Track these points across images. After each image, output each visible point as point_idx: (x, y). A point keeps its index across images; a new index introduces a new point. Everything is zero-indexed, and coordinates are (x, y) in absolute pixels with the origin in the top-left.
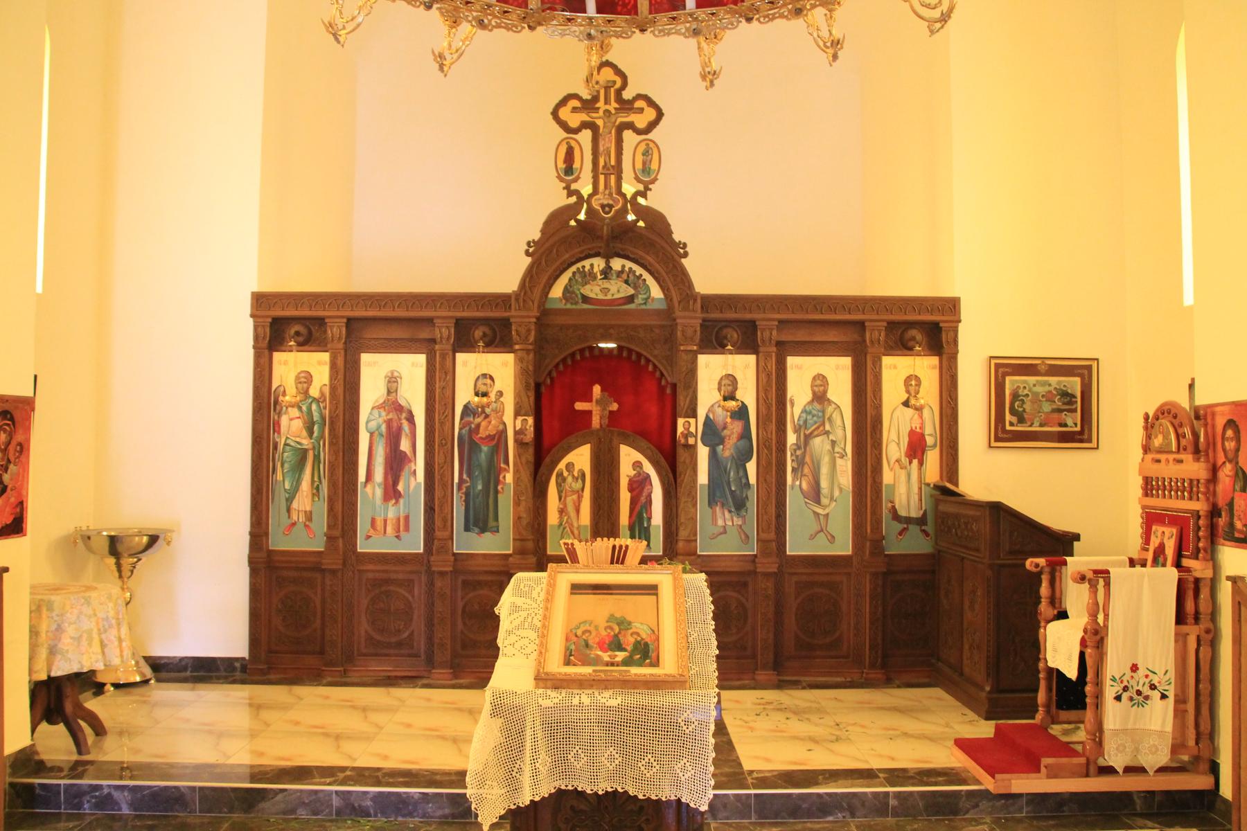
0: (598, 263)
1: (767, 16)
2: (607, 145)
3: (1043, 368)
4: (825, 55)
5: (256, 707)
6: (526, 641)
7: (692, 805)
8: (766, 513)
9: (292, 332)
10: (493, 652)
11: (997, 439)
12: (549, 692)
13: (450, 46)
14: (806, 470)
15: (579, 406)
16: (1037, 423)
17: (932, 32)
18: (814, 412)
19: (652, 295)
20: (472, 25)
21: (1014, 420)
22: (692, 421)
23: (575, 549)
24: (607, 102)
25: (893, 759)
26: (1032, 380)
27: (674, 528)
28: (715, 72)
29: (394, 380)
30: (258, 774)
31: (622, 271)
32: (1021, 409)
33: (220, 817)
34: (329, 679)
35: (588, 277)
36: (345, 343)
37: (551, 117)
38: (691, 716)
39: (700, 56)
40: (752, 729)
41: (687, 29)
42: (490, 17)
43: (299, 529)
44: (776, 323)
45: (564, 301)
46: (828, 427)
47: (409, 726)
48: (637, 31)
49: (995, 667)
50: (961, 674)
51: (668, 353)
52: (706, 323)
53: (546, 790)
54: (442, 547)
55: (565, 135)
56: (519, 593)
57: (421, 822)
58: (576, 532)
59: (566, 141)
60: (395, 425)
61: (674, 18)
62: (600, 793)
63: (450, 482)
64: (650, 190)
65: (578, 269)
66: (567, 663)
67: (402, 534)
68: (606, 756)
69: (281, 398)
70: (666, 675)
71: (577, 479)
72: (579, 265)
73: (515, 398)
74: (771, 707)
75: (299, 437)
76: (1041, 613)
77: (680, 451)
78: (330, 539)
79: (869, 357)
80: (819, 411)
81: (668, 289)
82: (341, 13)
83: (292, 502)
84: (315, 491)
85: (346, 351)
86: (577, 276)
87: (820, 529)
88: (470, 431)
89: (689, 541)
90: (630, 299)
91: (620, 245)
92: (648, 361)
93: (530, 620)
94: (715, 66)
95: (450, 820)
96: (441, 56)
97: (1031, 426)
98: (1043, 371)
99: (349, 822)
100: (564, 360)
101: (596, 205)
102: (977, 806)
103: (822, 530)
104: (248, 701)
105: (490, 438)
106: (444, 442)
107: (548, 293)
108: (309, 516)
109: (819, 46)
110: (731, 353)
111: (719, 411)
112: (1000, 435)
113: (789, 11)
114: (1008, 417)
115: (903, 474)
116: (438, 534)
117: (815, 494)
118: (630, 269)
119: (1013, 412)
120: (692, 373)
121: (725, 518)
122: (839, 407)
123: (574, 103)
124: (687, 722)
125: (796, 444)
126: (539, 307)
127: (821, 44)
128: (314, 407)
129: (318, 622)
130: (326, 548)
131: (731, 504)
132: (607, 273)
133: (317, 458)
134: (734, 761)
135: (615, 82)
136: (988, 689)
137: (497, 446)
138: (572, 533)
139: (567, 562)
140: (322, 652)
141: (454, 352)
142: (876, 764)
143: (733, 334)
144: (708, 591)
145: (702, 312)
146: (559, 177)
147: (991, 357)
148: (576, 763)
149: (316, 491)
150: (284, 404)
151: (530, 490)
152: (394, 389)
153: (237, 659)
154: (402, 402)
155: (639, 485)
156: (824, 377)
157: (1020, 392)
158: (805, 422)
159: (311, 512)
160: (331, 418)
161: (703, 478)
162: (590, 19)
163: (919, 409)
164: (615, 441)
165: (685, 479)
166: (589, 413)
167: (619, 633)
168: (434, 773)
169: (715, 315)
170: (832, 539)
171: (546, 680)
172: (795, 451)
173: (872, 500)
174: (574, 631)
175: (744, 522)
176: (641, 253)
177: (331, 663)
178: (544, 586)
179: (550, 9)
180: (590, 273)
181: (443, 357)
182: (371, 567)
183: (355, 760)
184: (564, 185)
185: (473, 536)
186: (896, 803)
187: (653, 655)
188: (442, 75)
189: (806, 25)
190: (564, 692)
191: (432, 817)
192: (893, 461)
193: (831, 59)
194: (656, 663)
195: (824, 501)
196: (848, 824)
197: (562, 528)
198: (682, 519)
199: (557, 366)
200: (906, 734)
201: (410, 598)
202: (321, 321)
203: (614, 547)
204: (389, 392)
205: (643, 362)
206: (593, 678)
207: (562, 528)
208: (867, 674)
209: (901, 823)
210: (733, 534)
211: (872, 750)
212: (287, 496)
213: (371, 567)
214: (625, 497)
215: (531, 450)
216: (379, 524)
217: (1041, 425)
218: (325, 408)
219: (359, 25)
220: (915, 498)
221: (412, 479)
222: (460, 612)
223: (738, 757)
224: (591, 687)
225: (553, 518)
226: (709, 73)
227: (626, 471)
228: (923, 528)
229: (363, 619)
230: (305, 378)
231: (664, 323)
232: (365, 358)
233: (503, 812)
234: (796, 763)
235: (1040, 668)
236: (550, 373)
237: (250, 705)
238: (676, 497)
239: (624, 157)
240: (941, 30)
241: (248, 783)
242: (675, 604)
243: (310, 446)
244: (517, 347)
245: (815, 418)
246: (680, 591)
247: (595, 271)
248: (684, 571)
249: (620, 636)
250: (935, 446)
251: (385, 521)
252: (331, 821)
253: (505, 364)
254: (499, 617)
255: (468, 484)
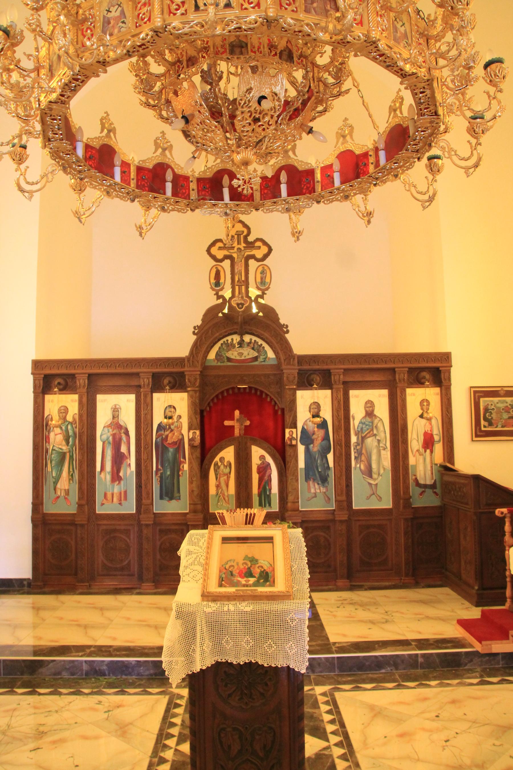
0: (236, 338)
1: (329, 200)
2: (239, 269)
3: (502, 393)
4: (363, 221)
5: (37, 609)
6: (196, 572)
7: (296, 669)
8: (340, 484)
9: (56, 383)
10: (177, 579)
11: (477, 436)
12: (210, 603)
13: (145, 221)
14: (363, 458)
15: (227, 423)
16: (500, 426)
17: (424, 208)
18: (367, 423)
19: (268, 356)
20: (158, 210)
21: (486, 424)
22: (294, 430)
23: (224, 516)
24: (239, 243)
25: (420, 633)
26: (496, 400)
27: (285, 495)
28: (300, 231)
29: (116, 410)
30: (38, 651)
31: (250, 343)
32: (490, 418)
33: (15, 678)
34: (80, 591)
35: (230, 346)
36: (87, 388)
37: (206, 253)
38: (294, 616)
39: (291, 223)
40: (335, 616)
41: (283, 208)
42: (168, 205)
43: (62, 500)
44: (342, 371)
45: (216, 361)
46: (375, 432)
47: (128, 619)
48: (254, 210)
49: (480, 575)
50: (460, 579)
51: (279, 390)
52: (301, 372)
53: (209, 662)
54: (147, 509)
55: (215, 263)
56: (191, 543)
57: (136, 679)
58: (226, 498)
59: (215, 267)
60: (118, 437)
61: (275, 202)
62: (242, 663)
63: (151, 471)
64: (266, 294)
65: (224, 342)
66: (221, 585)
67: (123, 502)
68: (245, 641)
69: (50, 422)
70: (279, 592)
71: (226, 467)
72: (225, 339)
73: (188, 419)
74: (345, 602)
75: (61, 445)
76: (506, 542)
77: (287, 448)
78: (80, 506)
79: (398, 389)
80: (370, 422)
81: (278, 353)
82: (82, 205)
83: (57, 484)
84: (70, 477)
85: (88, 393)
86: (224, 346)
87: (372, 493)
88: (163, 440)
89: (294, 502)
90: (256, 359)
91: (249, 327)
92: (267, 395)
93: (198, 559)
94: (299, 228)
95: (154, 677)
96: (141, 227)
97: (496, 427)
98: (502, 394)
99: (93, 679)
100: (217, 396)
101: (234, 304)
102: (471, 661)
103: (374, 494)
104: (31, 605)
105: (174, 443)
106: (147, 446)
107: (207, 356)
108: (67, 492)
109: (359, 216)
110: (316, 389)
111: (310, 424)
112: (478, 433)
113: (341, 197)
114: (483, 422)
115: (421, 459)
116: (144, 501)
117: (369, 472)
118: (255, 341)
119: (485, 419)
120: (293, 402)
121: (315, 488)
122: (381, 419)
123: (220, 244)
124: (292, 620)
125: (357, 443)
126: (202, 365)
127: (361, 215)
128: (69, 427)
129: (73, 556)
130: (78, 511)
131: (319, 479)
132: (241, 344)
133: (71, 457)
134: (324, 636)
135: (243, 232)
136: (476, 588)
137: (179, 447)
138: (224, 499)
139: (219, 524)
140: (76, 574)
141: (152, 392)
142: (410, 636)
143: (317, 378)
144: (303, 539)
145: (298, 366)
146: (212, 288)
147: (471, 387)
148: (227, 646)
149: (71, 477)
150: (51, 426)
151: (199, 475)
152: (117, 415)
153: (25, 580)
154: (122, 423)
155: (264, 469)
156: (372, 402)
157: (489, 407)
158: (362, 429)
159: (68, 490)
160: (79, 433)
161: (302, 464)
162: (226, 204)
163: (429, 420)
164: (248, 444)
165: (290, 465)
166: (233, 427)
167: (251, 566)
168: (144, 648)
169: (306, 367)
170: (380, 499)
171: (208, 596)
172: (356, 446)
173: (403, 475)
174: (224, 566)
175: (327, 490)
176: (262, 332)
177: (82, 581)
178: (206, 538)
179: (202, 199)
180: (231, 344)
181: (145, 396)
182: (105, 522)
183: (96, 641)
184: (215, 292)
185: (165, 502)
186: (423, 660)
187: (272, 580)
188: (141, 238)
189: (351, 205)
190: (219, 603)
191: (142, 675)
192: (415, 451)
193: (367, 223)
194: (273, 584)
195: (375, 476)
196: (394, 674)
197: (218, 496)
198: (290, 489)
199: (213, 400)
200: (428, 618)
201: (128, 540)
202: (73, 376)
203: (247, 515)
204: (114, 417)
205: (264, 396)
206: (235, 594)
207: (218, 496)
208: (404, 580)
209: (426, 673)
210: (320, 497)
211: (408, 627)
212: (54, 480)
213: (105, 522)
214: (255, 477)
215: (199, 450)
216: (109, 496)
217: (502, 427)
218: (76, 427)
219: (93, 212)
220: (429, 472)
221: (128, 469)
222: (158, 547)
223: (326, 634)
224: (235, 600)
225: (212, 490)
226: (296, 232)
227: (255, 461)
228: (435, 490)
229: (101, 554)
230: (64, 410)
231: (275, 372)
232: (100, 397)
233: (184, 676)
234: (361, 637)
235: (507, 575)
236: (209, 404)
237: (33, 608)
238: (286, 477)
239: (250, 275)
240: (429, 207)
241: (31, 656)
242: (284, 548)
243: (68, 450)
244: (189, 389)
245: (367, 427)
246: (286, 539)
247: (234, 342)
248: (289, 527)
249: (251, 568)
250: (439, 441)
251: (113, 494)
252: (83, 679)
253: (182, 399)
254: (180, 557)
255: (162, 471)
